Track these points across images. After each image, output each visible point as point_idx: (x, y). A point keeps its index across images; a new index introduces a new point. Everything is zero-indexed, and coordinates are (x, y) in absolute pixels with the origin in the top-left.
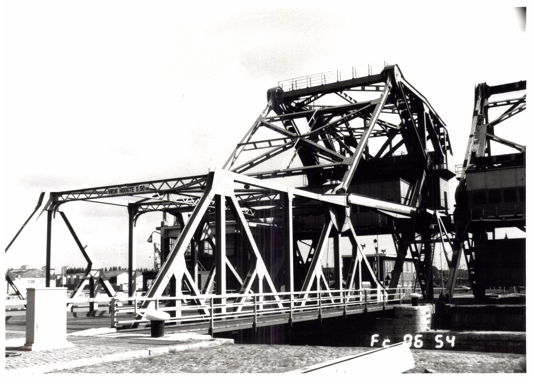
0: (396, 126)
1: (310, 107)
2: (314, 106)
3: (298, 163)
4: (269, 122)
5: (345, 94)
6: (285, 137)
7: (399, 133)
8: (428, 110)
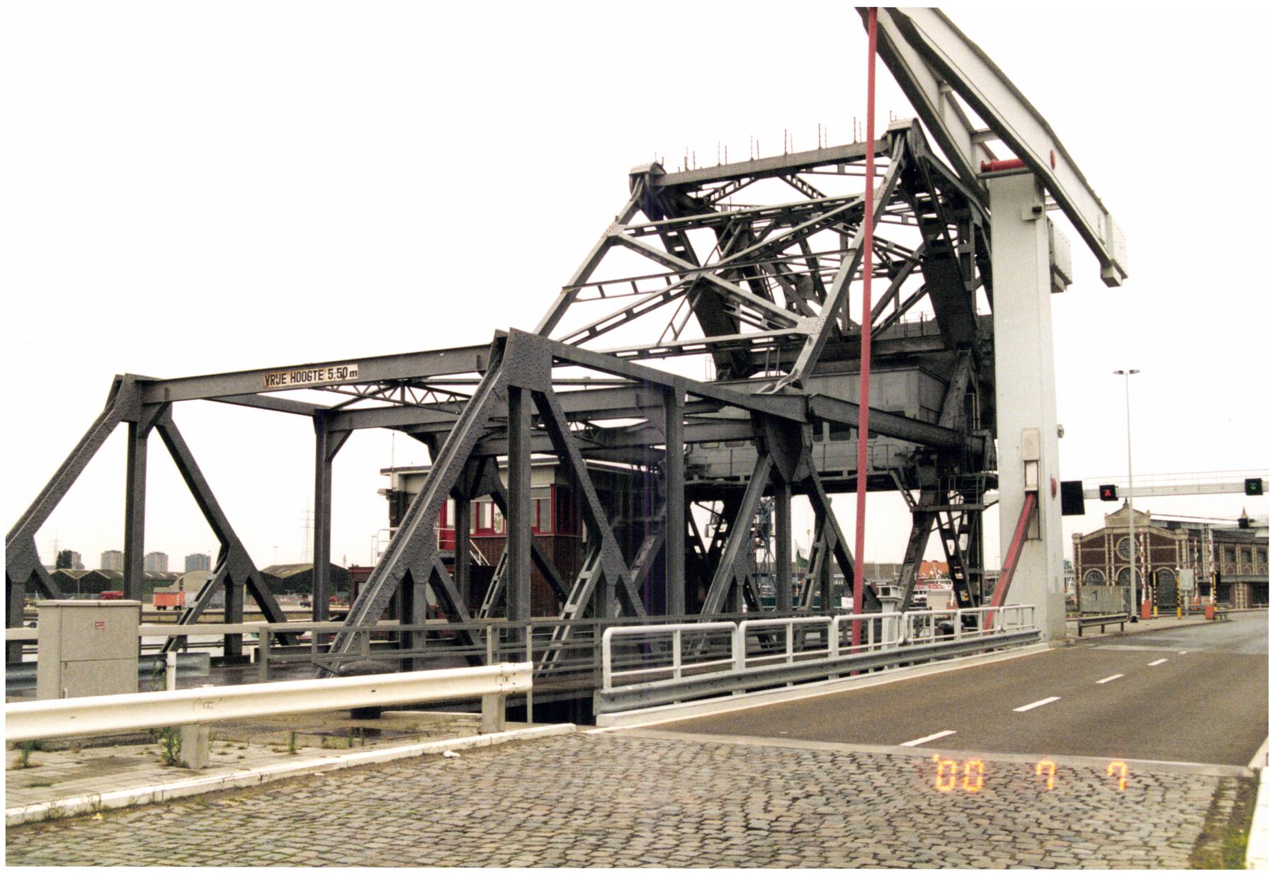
0: (910, 252)
1: (724, 207)
2: (731, 206)
3: (694, 332)
4: (633, 235)
5: (800, 180)
6: (667, 270)
7: (918, 272)
8: (980, 218)
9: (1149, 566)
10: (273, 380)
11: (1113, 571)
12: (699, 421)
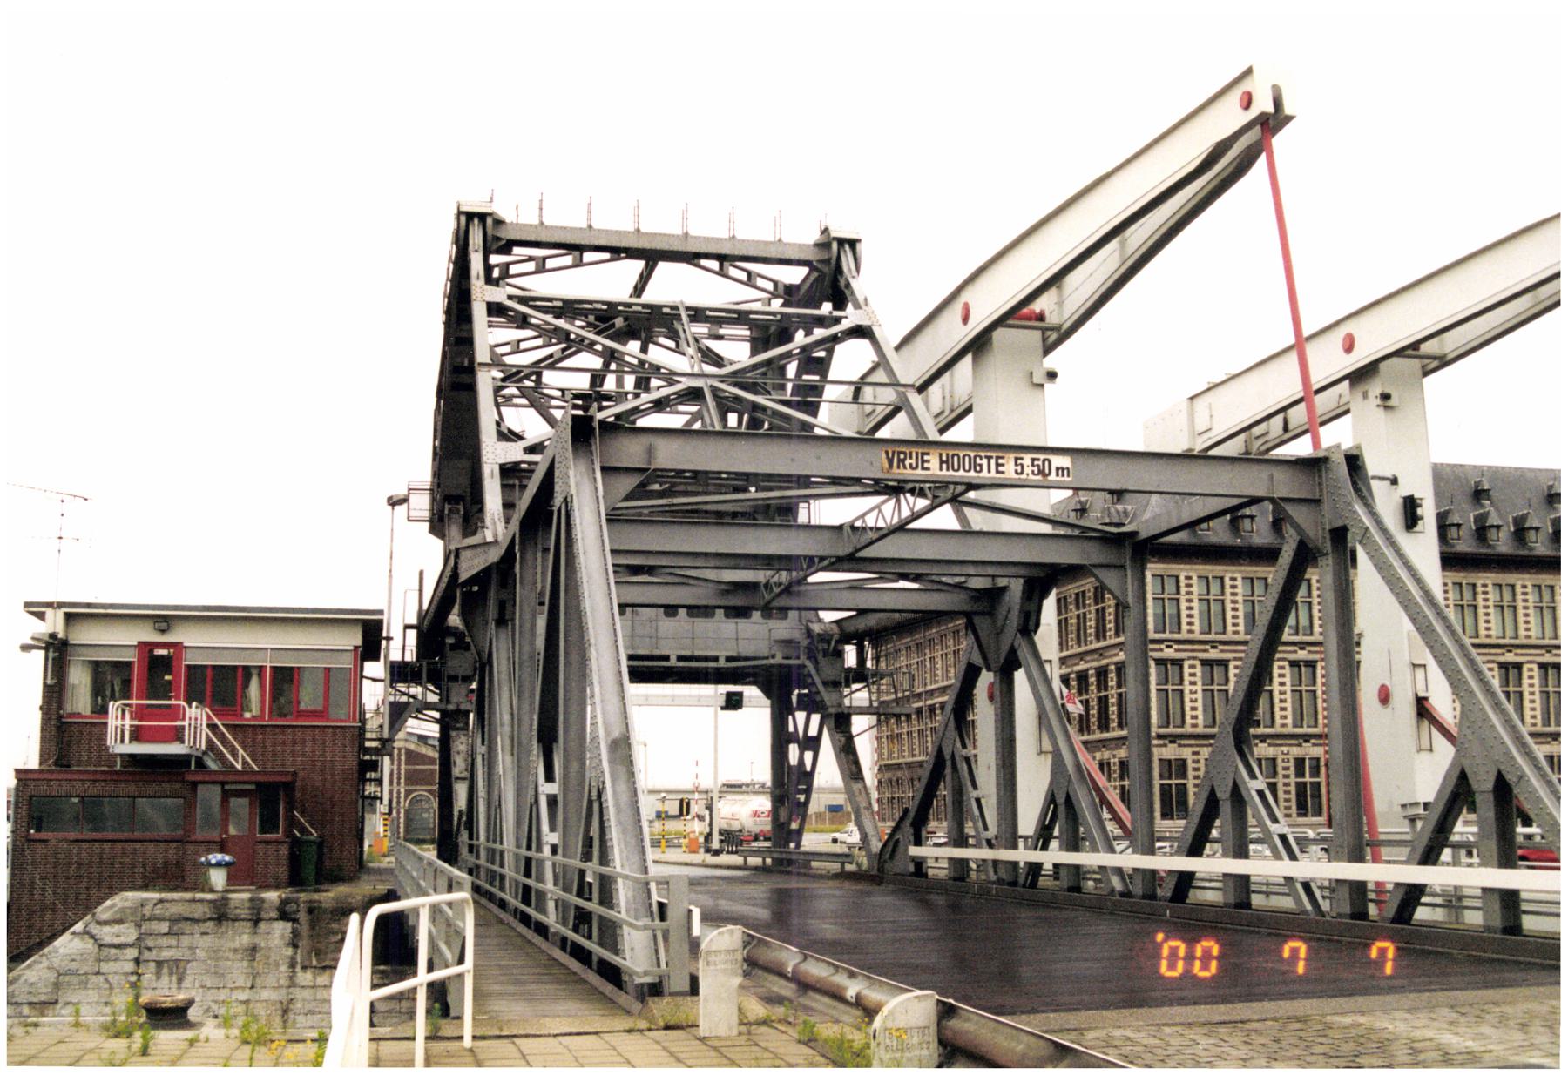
9: (402, 790)
10: (902, 461)
11: (402, 795)
12: (677, 580)
